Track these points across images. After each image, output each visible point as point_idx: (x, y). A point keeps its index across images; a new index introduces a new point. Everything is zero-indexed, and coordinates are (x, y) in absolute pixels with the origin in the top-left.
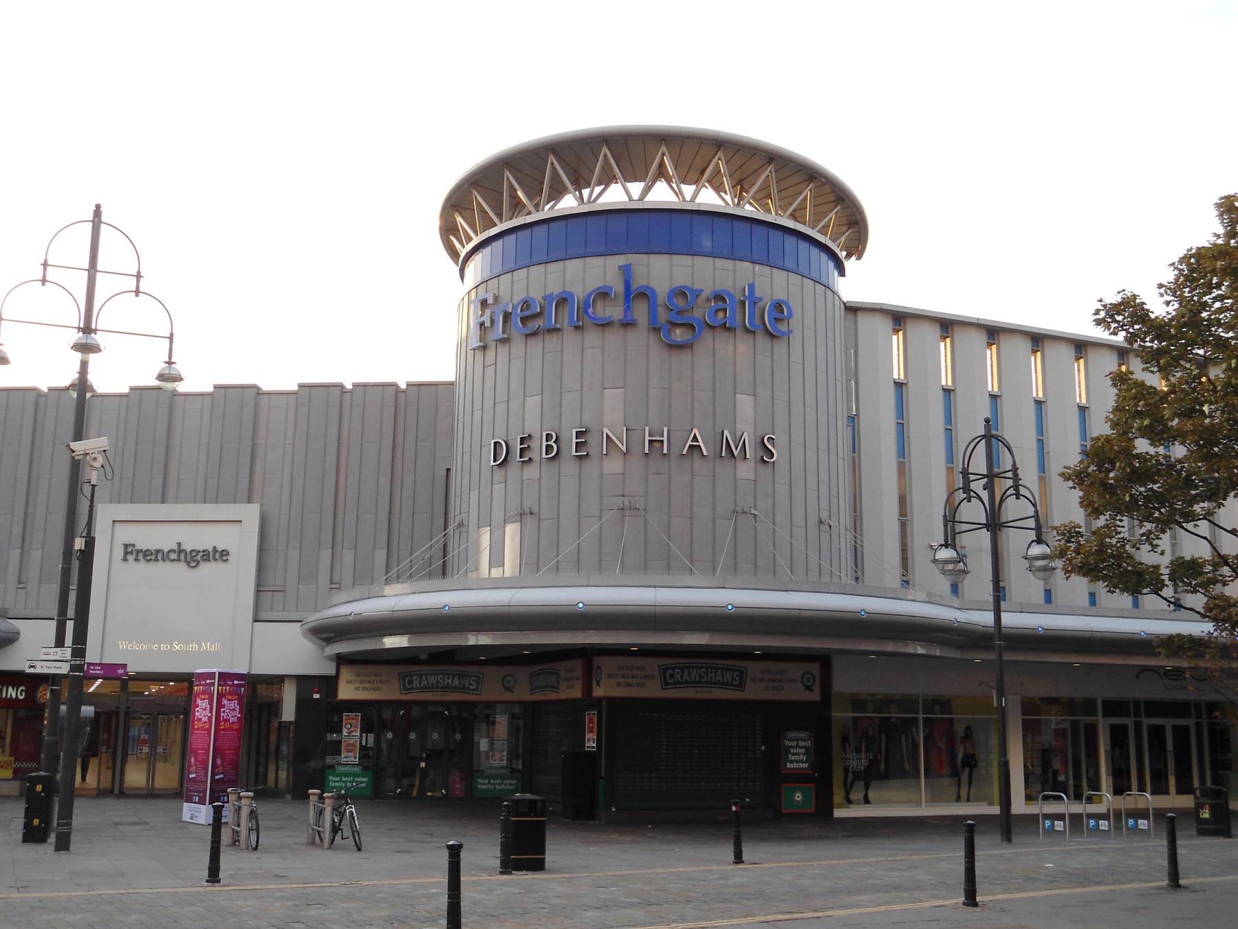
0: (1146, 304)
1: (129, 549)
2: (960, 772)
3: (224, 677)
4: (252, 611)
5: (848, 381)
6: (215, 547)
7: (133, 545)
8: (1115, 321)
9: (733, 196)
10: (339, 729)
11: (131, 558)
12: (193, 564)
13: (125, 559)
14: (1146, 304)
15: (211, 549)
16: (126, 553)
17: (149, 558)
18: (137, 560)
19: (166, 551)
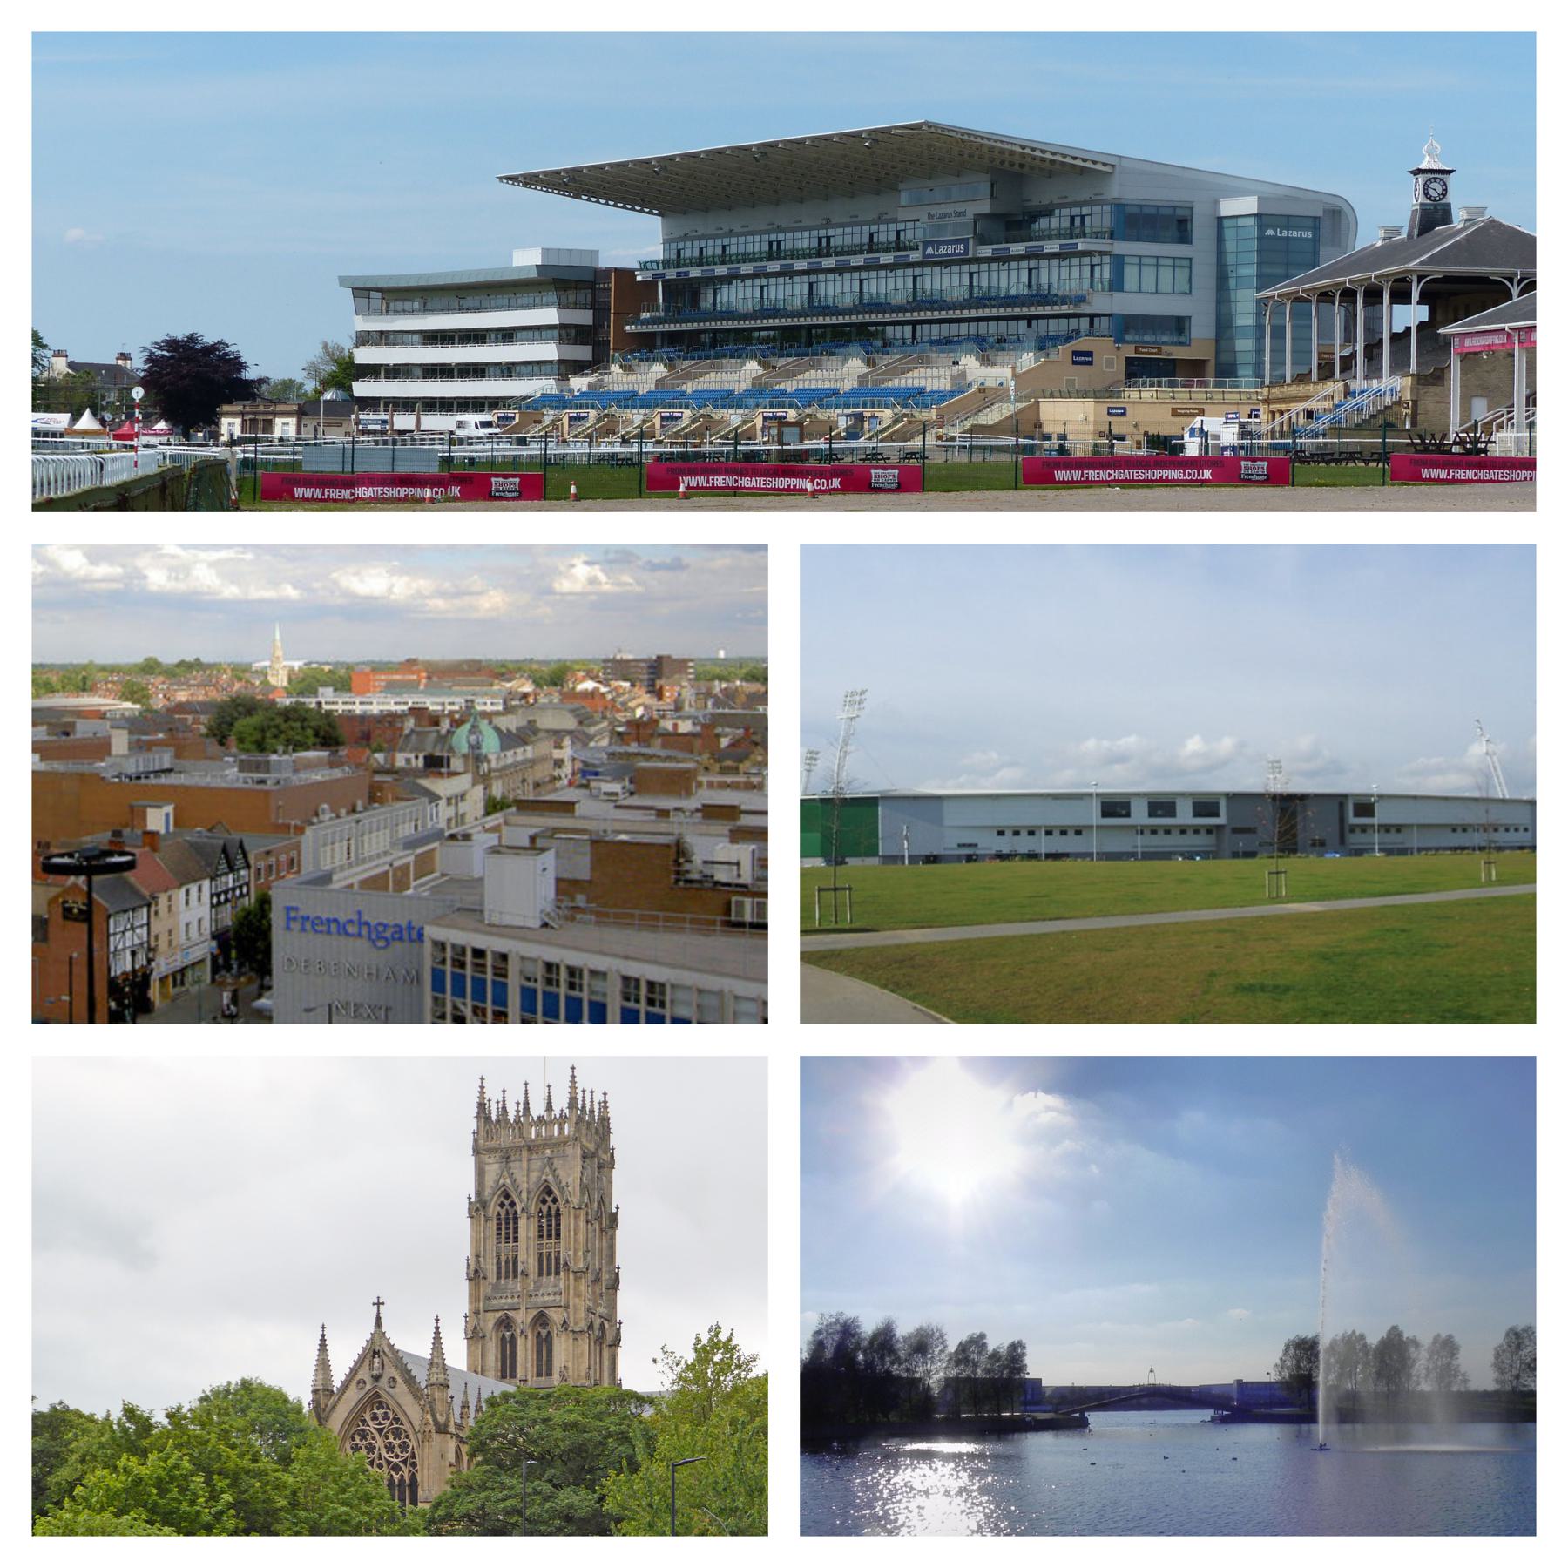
0: (698, 1340)
1: (293, 914)
2: (50, 571)
3: (605, 661)
4: (1036, 493)
5: (66, 446)
6: (410, 923)
7: (296, 909)
8: (704, 1450)
9: (341, 748)
10: (563, 885)
11: (296, 926)
12: (381, 943)
13: (288, 928)
14: (698, 1340)
15: (404, 924)
16: (289, 919)
17: (319, 928)
18: (303, 930)
19: (342, 920)
